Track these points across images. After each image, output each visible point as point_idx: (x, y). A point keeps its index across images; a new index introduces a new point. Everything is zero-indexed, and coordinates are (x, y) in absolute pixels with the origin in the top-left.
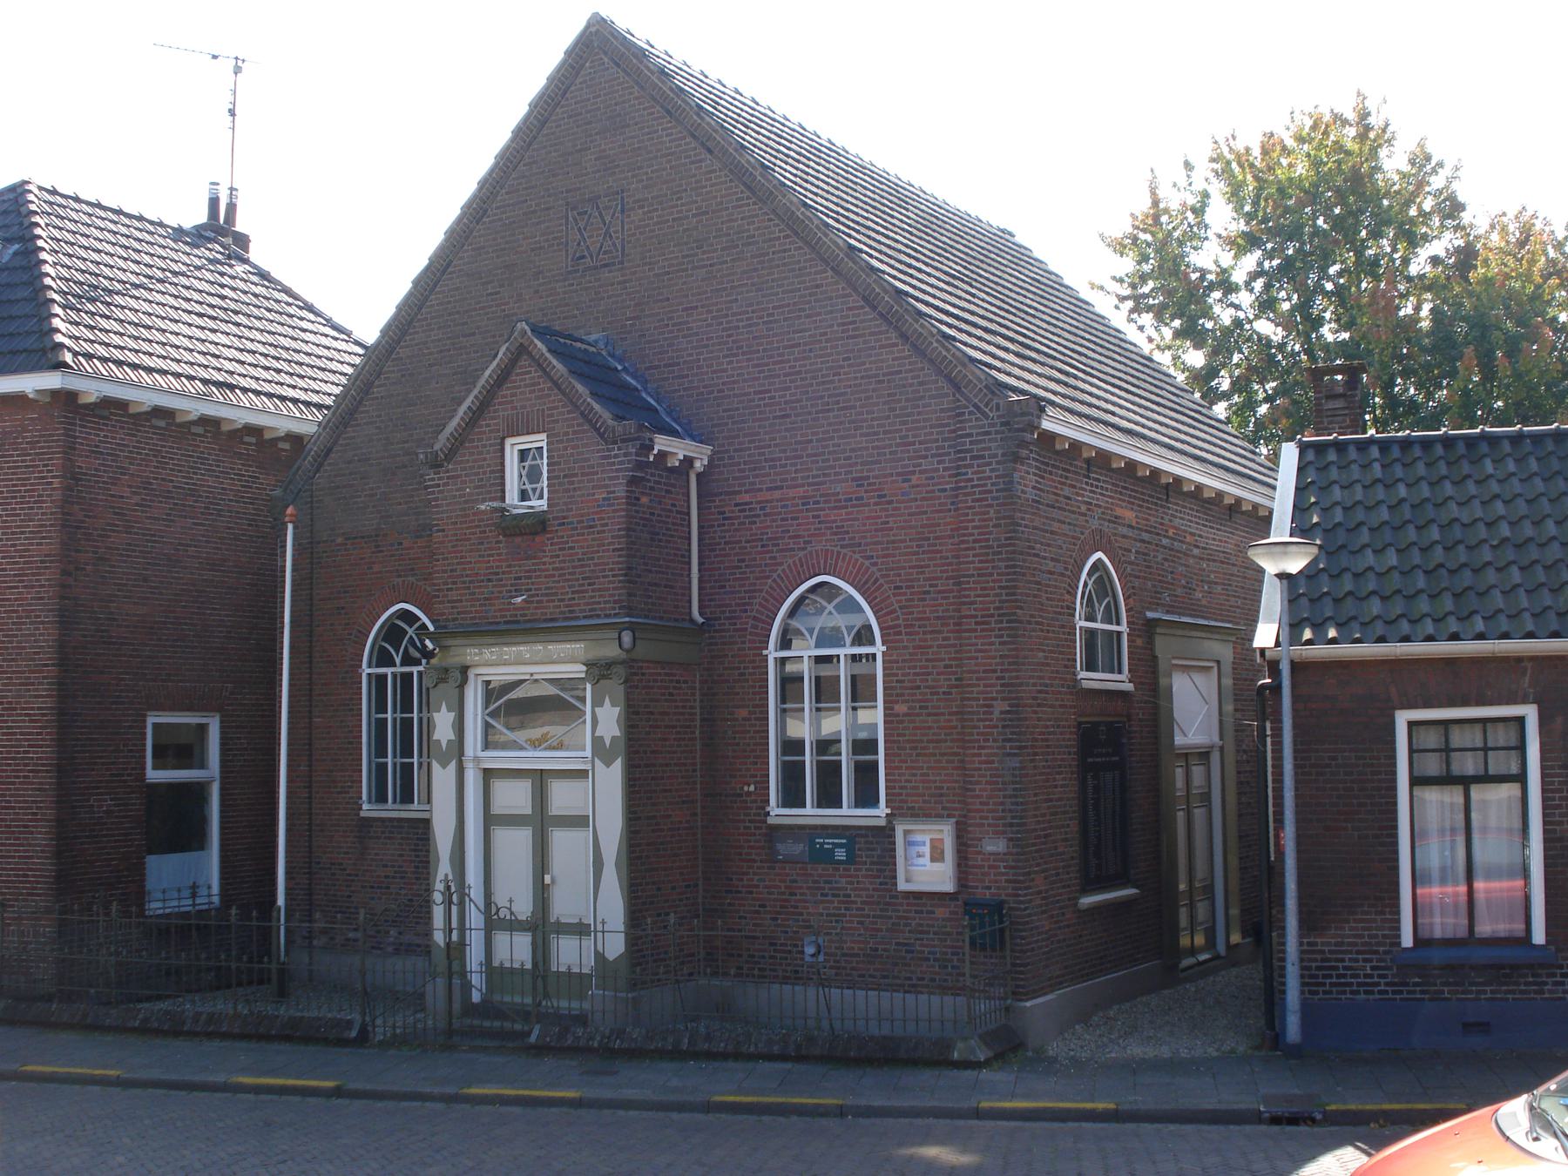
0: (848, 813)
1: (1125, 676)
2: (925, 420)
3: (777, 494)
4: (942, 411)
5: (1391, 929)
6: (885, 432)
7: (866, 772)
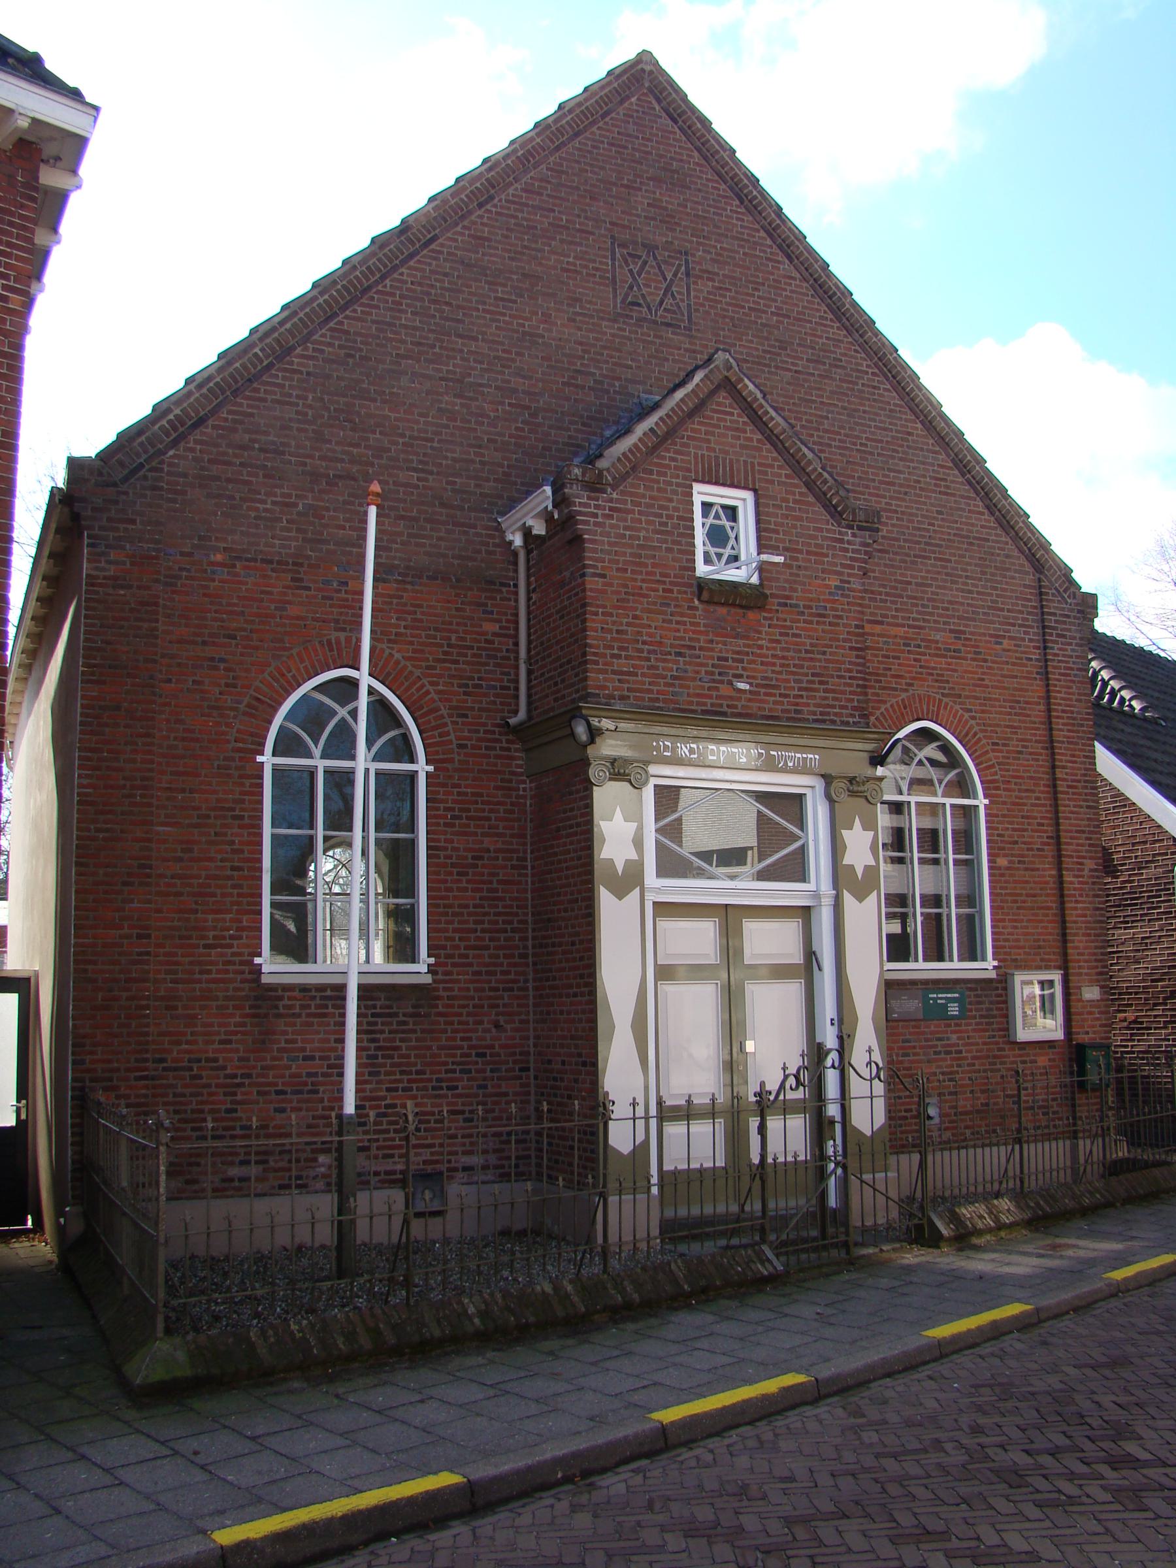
0: (954, 967)
2: (1012, 591)
3: (878, 629)
4: (1025, 586)
6: (978, 593)
7: (970, 926)
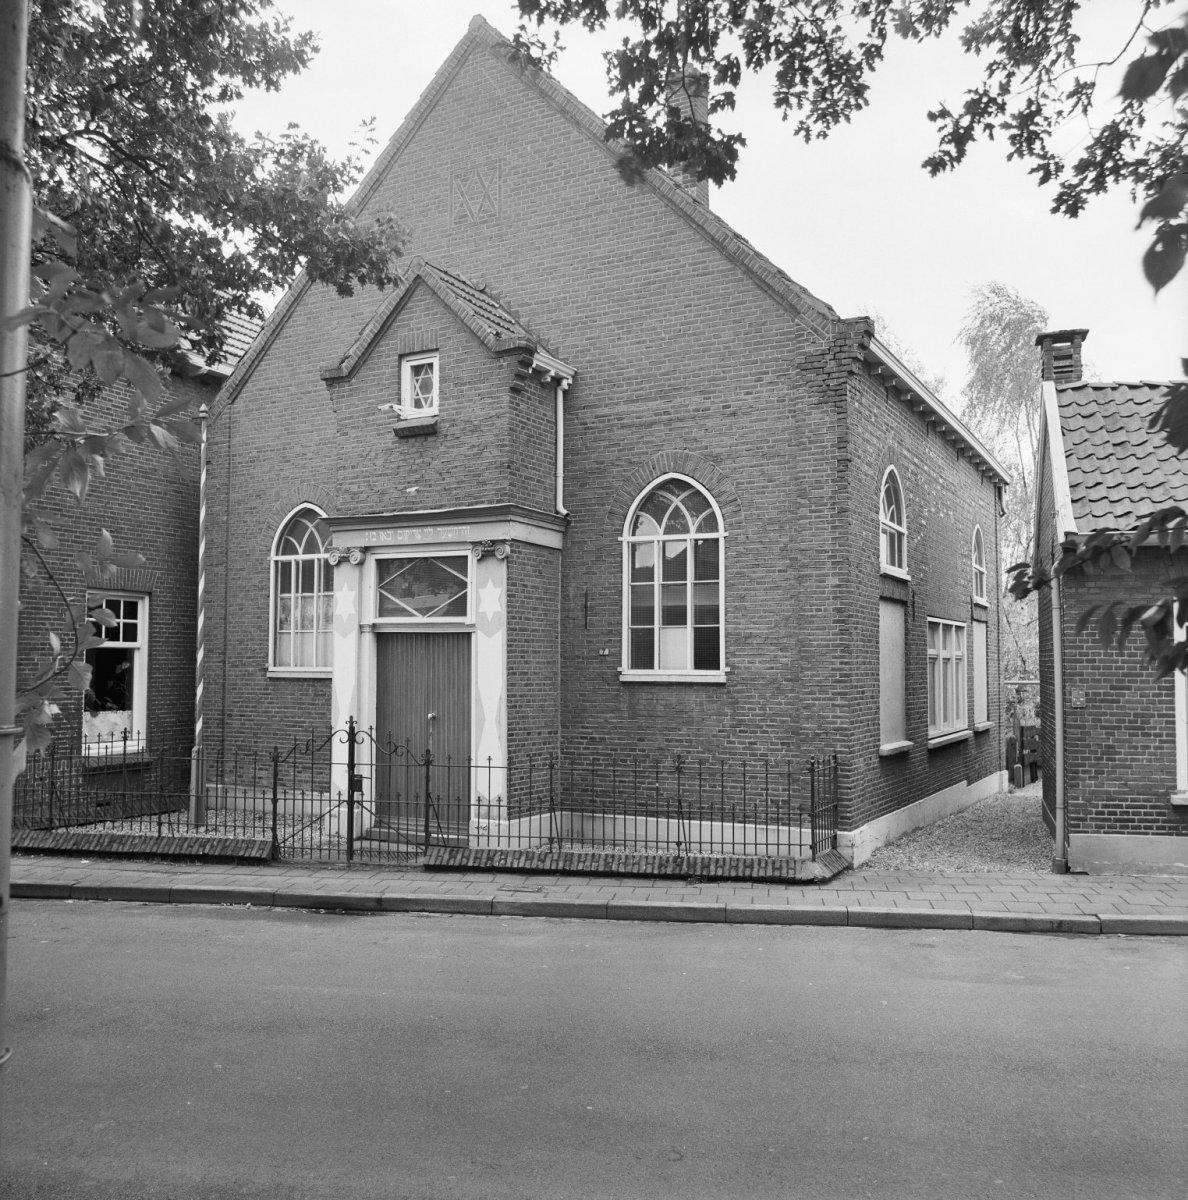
1: (906, 569)
5: (1168, 773)
